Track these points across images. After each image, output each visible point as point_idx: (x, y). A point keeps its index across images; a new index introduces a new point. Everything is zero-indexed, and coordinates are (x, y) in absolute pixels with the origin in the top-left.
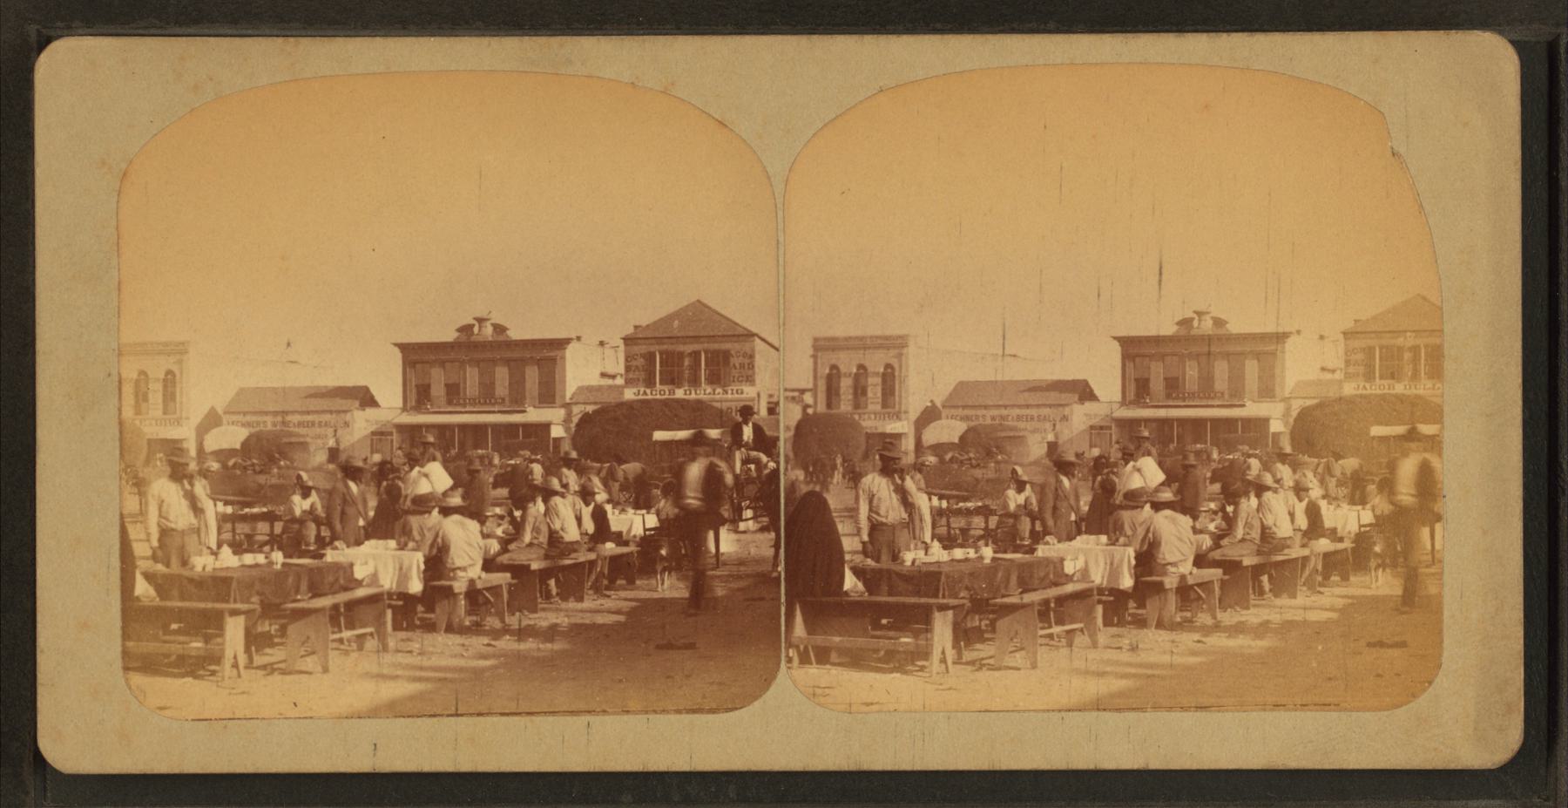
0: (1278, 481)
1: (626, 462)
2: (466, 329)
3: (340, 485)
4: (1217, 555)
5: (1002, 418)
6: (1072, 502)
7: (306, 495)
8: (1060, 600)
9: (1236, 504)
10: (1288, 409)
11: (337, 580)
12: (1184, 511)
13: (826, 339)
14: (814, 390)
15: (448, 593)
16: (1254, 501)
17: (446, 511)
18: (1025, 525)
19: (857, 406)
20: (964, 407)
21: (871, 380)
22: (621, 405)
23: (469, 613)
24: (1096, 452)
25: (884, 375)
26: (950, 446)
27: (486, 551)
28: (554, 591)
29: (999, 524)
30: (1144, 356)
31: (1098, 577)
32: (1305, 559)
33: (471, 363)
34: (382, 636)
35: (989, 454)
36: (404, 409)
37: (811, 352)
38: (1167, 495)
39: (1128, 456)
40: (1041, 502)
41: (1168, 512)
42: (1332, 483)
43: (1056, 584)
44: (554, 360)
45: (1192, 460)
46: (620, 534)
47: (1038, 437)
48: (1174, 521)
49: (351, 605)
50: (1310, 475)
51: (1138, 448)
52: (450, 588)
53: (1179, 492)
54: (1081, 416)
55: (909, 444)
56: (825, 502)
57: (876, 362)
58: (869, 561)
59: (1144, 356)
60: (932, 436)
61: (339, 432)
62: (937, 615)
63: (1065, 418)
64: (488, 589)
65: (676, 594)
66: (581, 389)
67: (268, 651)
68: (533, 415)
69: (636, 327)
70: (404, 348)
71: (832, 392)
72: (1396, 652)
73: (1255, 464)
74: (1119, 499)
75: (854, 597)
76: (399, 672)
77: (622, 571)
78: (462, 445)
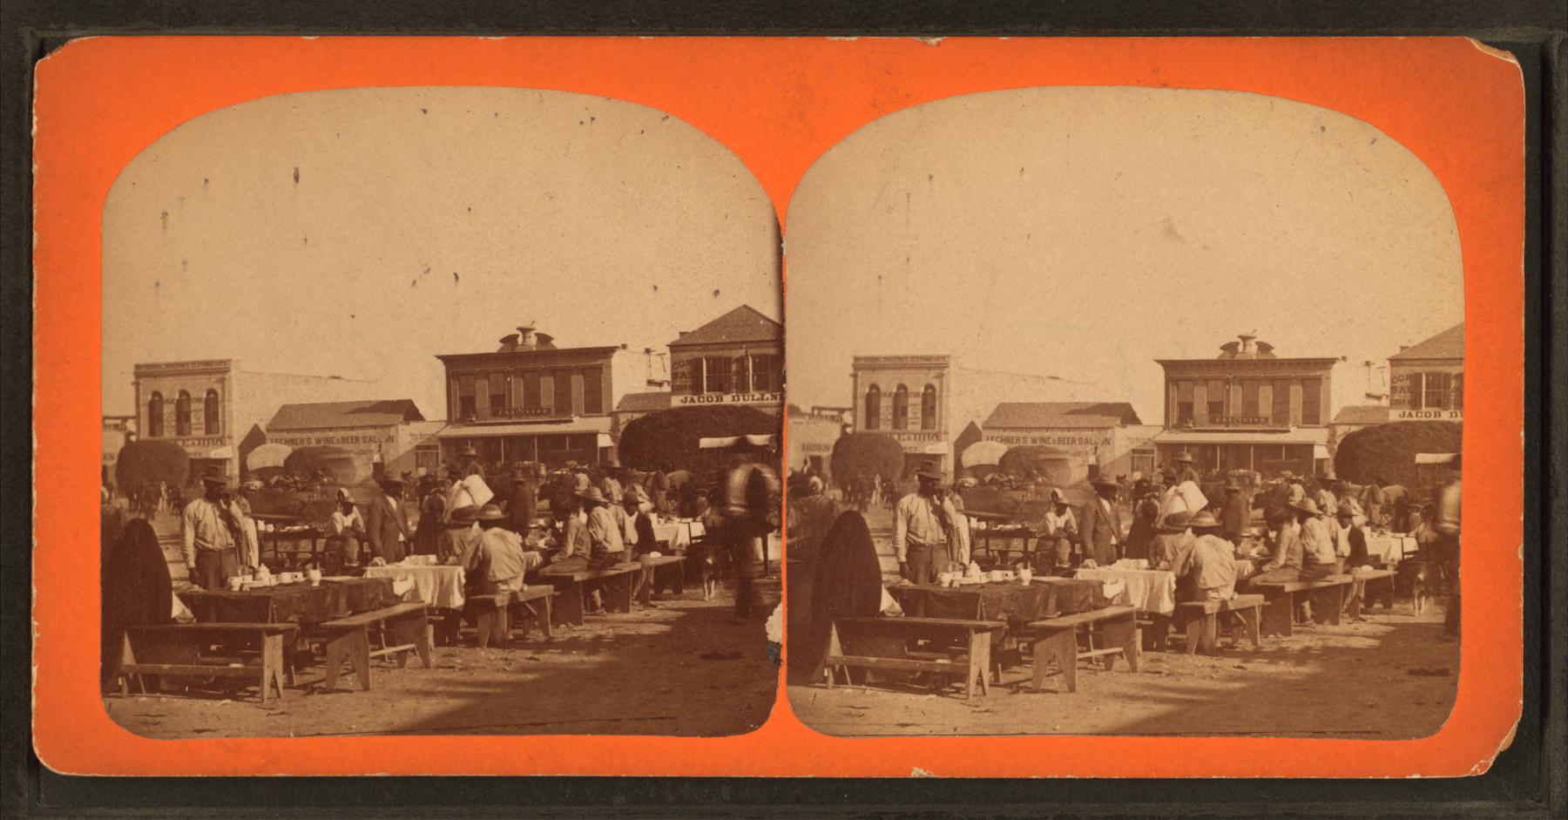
0: (1321, 508)
1: (1387, 484)
2: (1230, 347)
3: (1093, 503)
4: (1258, 580)
5: (328, 440)
6: (1113, 525)
7: (347, 512)
8: (1099, 623)
9: (1279, 530)
10: (1333, 435)
11: (377, 596)
12: (513, 529)
13: (866, 359)
14: (854, 409)
15: (1199, 613)
16: (1296, 527)
17: (486, 524)
18: (1065, 549)
19: (180, 432)
20: (288, 431)
21: (194, 406)
22: (1385, 427)
23: (511, 627)
24: (1138, 476)
25: (179, 401)
26: (990, 468)
27: (529, 564)
28: (599, 602)
29: (327, 546)
30: (1190, 380)
31: (1138, 601)
32: (1348, 586)
33: (517, 378)
34: (423, 650)
35: (1029, 476)
36: (1166, 427)
37: (133, 379)
38: (496, 513)
39: (1170, 481)
40: (1081, 525)
41: (497, 530)
42: (1376, 509)
43: (1096, 608)
44: (1318, 379)
45: (1235, 486)
46: (1377, 557)
47: (1080, 459)
48: (503, 538)
49: (392, 621)
50: (1354, 502)
51: (1180, 472)
52: (1202, 609)
53: (1220, 518)
54: (1123, 440)
55: (948, 465)
56: (863, 520)
57: (916, 383)
58: (906, 582)
59: (1190, 380)
60: (971, 457)
61: (384, 447)
62: (268, 641)
63: (391, 439)
64: (530, 602)
65: (1433, 620)
66: (628, 398)
67: (1015, 668)
68: (579, 424)
69: (682, 334)
70: (1168, 365)
71: (872, 411)
72: (1439, 679)
73: (1298, 490)
74: (1160, 523)
75: (890, 617)
76: (1146, 693)
77: (1385, 592)
78: (1223, 464)
